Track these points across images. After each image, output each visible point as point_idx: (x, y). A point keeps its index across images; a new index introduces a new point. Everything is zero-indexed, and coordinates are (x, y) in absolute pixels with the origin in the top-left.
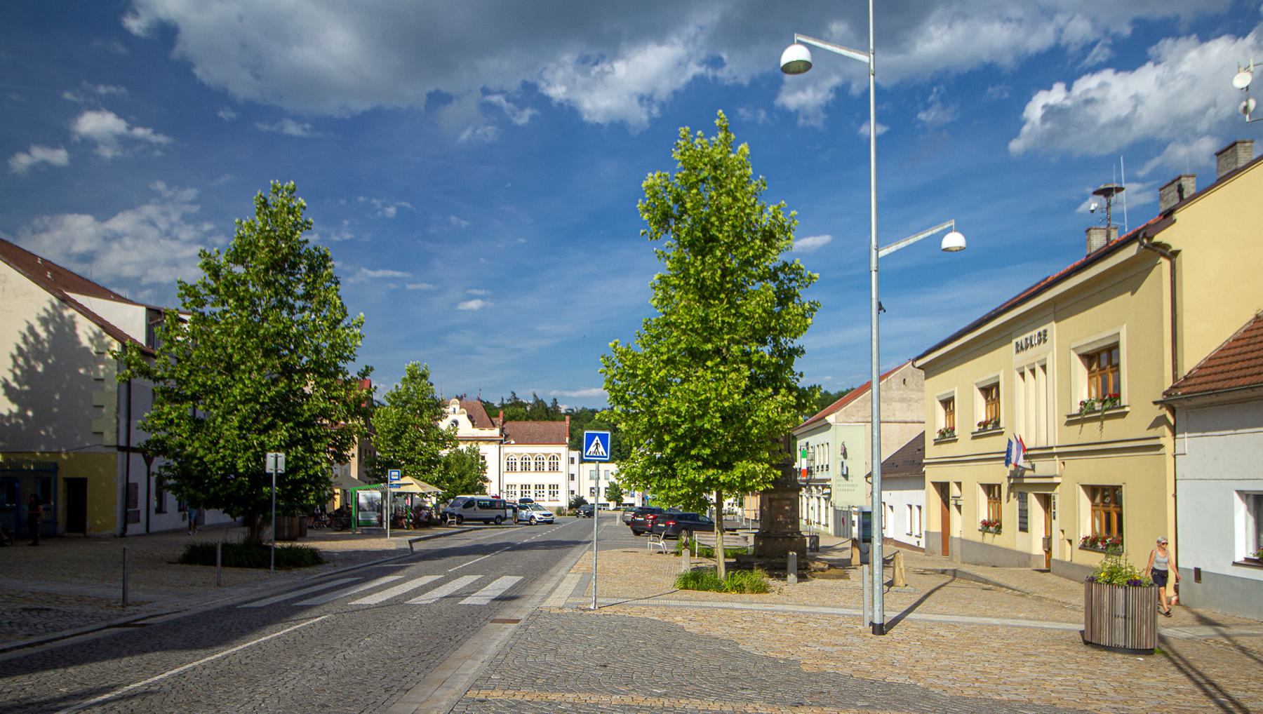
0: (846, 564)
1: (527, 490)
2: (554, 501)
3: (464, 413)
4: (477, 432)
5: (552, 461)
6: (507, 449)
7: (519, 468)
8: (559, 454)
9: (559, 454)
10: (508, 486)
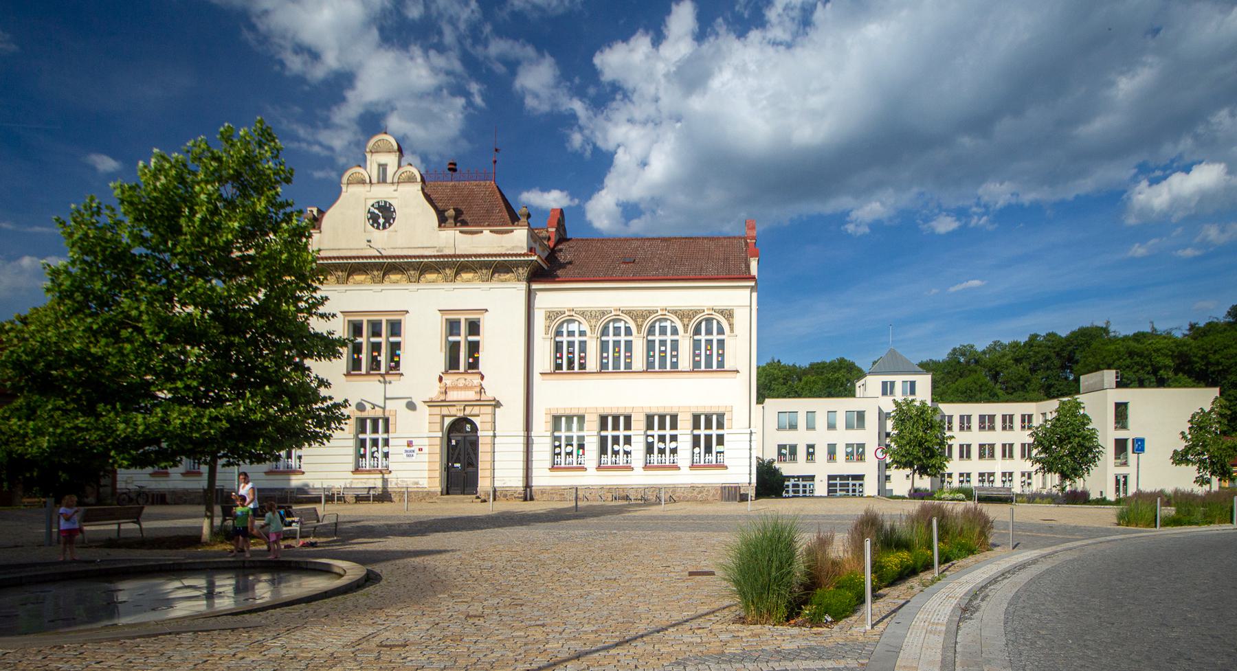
0: (107, 207)
1: (622, 433)
2: (708, 466)
3: (411, 180)
4: (454, 241)
5: (703, 337)
6: (551, 299)
7: (592, 363)
8: (728, 314)
9: (728, 314)
10: (556, 419)
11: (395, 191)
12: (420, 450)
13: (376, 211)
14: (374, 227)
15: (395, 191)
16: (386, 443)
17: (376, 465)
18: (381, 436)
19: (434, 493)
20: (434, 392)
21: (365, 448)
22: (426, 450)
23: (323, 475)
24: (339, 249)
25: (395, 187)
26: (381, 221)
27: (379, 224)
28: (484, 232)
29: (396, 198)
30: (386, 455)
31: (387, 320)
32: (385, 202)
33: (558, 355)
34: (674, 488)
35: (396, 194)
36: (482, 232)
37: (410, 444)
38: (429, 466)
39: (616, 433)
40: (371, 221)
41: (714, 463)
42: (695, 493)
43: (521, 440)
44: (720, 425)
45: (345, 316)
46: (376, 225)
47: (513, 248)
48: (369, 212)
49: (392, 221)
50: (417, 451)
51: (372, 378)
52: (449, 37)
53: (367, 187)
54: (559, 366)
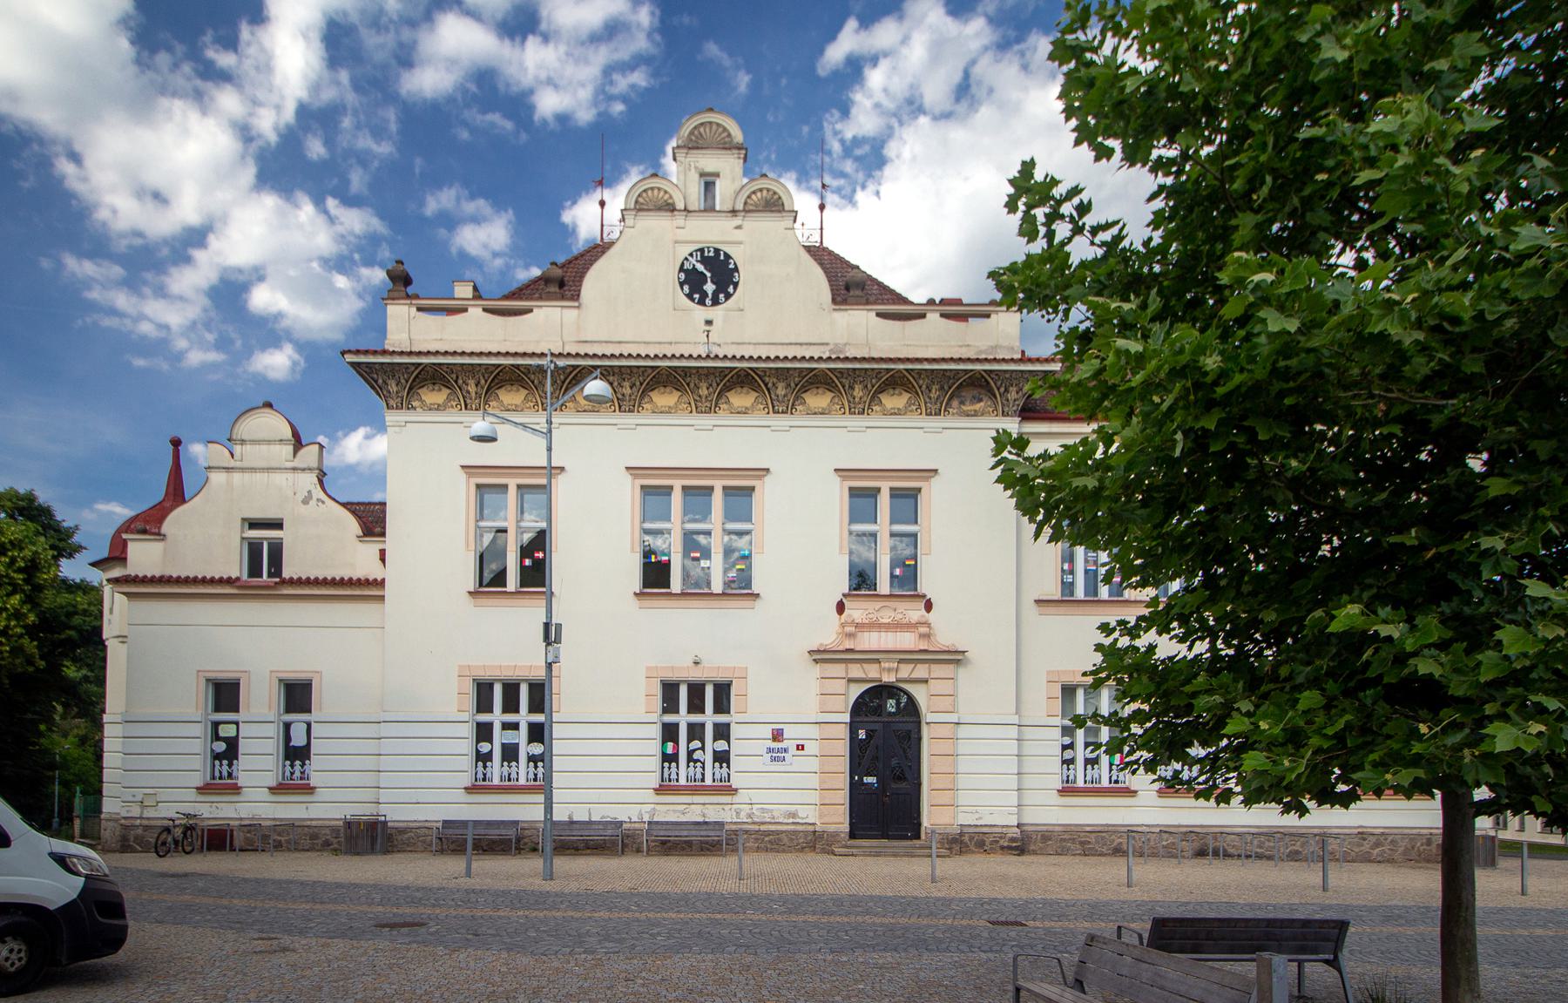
2: (696, 788)
11: (739, 227)
12: (800, 747)
13: (700, 267)
14: (693, 300)
15: (739, 227)
16: (722, 732)
17: (699, 776)
18: (709, 718)
19: (835, 834)
20: (828, 634)
21: (676, 742)
22: (812, 747)
23: (592, 795)
24: (620, 342)
25: (737, 221)
26: (709, 288)
27: (704, 295)
28: (928, 315)
29: (741, 243)
30: (722, 758)
31: (892, 489)
32: (717, 251)
33: (1066, 567)
34: (1131, 832)
35: (738, 235)
36: (988, 316)
37: (777, 736)
38: (821, 782)
39: (696, 718)
40: (686, 288)
41: (1105, 783)
42: (1366, 847)
43: (313, 735)
44: (722, 705)
45: (469, 475)
46: (697, 296)
47: (995, 348)
48: (681, 269)
49: (731, 289)
50: (793, 750)
51: (526, 601)
52: (358, 180)
53: (680, 220)
54: (1068, 588)
